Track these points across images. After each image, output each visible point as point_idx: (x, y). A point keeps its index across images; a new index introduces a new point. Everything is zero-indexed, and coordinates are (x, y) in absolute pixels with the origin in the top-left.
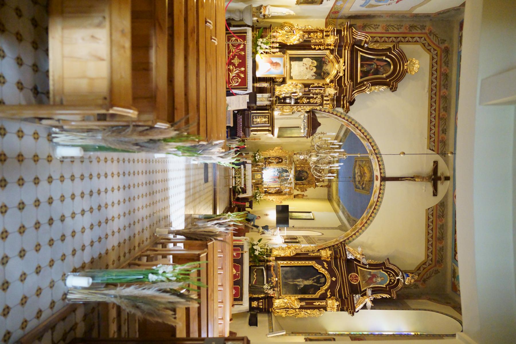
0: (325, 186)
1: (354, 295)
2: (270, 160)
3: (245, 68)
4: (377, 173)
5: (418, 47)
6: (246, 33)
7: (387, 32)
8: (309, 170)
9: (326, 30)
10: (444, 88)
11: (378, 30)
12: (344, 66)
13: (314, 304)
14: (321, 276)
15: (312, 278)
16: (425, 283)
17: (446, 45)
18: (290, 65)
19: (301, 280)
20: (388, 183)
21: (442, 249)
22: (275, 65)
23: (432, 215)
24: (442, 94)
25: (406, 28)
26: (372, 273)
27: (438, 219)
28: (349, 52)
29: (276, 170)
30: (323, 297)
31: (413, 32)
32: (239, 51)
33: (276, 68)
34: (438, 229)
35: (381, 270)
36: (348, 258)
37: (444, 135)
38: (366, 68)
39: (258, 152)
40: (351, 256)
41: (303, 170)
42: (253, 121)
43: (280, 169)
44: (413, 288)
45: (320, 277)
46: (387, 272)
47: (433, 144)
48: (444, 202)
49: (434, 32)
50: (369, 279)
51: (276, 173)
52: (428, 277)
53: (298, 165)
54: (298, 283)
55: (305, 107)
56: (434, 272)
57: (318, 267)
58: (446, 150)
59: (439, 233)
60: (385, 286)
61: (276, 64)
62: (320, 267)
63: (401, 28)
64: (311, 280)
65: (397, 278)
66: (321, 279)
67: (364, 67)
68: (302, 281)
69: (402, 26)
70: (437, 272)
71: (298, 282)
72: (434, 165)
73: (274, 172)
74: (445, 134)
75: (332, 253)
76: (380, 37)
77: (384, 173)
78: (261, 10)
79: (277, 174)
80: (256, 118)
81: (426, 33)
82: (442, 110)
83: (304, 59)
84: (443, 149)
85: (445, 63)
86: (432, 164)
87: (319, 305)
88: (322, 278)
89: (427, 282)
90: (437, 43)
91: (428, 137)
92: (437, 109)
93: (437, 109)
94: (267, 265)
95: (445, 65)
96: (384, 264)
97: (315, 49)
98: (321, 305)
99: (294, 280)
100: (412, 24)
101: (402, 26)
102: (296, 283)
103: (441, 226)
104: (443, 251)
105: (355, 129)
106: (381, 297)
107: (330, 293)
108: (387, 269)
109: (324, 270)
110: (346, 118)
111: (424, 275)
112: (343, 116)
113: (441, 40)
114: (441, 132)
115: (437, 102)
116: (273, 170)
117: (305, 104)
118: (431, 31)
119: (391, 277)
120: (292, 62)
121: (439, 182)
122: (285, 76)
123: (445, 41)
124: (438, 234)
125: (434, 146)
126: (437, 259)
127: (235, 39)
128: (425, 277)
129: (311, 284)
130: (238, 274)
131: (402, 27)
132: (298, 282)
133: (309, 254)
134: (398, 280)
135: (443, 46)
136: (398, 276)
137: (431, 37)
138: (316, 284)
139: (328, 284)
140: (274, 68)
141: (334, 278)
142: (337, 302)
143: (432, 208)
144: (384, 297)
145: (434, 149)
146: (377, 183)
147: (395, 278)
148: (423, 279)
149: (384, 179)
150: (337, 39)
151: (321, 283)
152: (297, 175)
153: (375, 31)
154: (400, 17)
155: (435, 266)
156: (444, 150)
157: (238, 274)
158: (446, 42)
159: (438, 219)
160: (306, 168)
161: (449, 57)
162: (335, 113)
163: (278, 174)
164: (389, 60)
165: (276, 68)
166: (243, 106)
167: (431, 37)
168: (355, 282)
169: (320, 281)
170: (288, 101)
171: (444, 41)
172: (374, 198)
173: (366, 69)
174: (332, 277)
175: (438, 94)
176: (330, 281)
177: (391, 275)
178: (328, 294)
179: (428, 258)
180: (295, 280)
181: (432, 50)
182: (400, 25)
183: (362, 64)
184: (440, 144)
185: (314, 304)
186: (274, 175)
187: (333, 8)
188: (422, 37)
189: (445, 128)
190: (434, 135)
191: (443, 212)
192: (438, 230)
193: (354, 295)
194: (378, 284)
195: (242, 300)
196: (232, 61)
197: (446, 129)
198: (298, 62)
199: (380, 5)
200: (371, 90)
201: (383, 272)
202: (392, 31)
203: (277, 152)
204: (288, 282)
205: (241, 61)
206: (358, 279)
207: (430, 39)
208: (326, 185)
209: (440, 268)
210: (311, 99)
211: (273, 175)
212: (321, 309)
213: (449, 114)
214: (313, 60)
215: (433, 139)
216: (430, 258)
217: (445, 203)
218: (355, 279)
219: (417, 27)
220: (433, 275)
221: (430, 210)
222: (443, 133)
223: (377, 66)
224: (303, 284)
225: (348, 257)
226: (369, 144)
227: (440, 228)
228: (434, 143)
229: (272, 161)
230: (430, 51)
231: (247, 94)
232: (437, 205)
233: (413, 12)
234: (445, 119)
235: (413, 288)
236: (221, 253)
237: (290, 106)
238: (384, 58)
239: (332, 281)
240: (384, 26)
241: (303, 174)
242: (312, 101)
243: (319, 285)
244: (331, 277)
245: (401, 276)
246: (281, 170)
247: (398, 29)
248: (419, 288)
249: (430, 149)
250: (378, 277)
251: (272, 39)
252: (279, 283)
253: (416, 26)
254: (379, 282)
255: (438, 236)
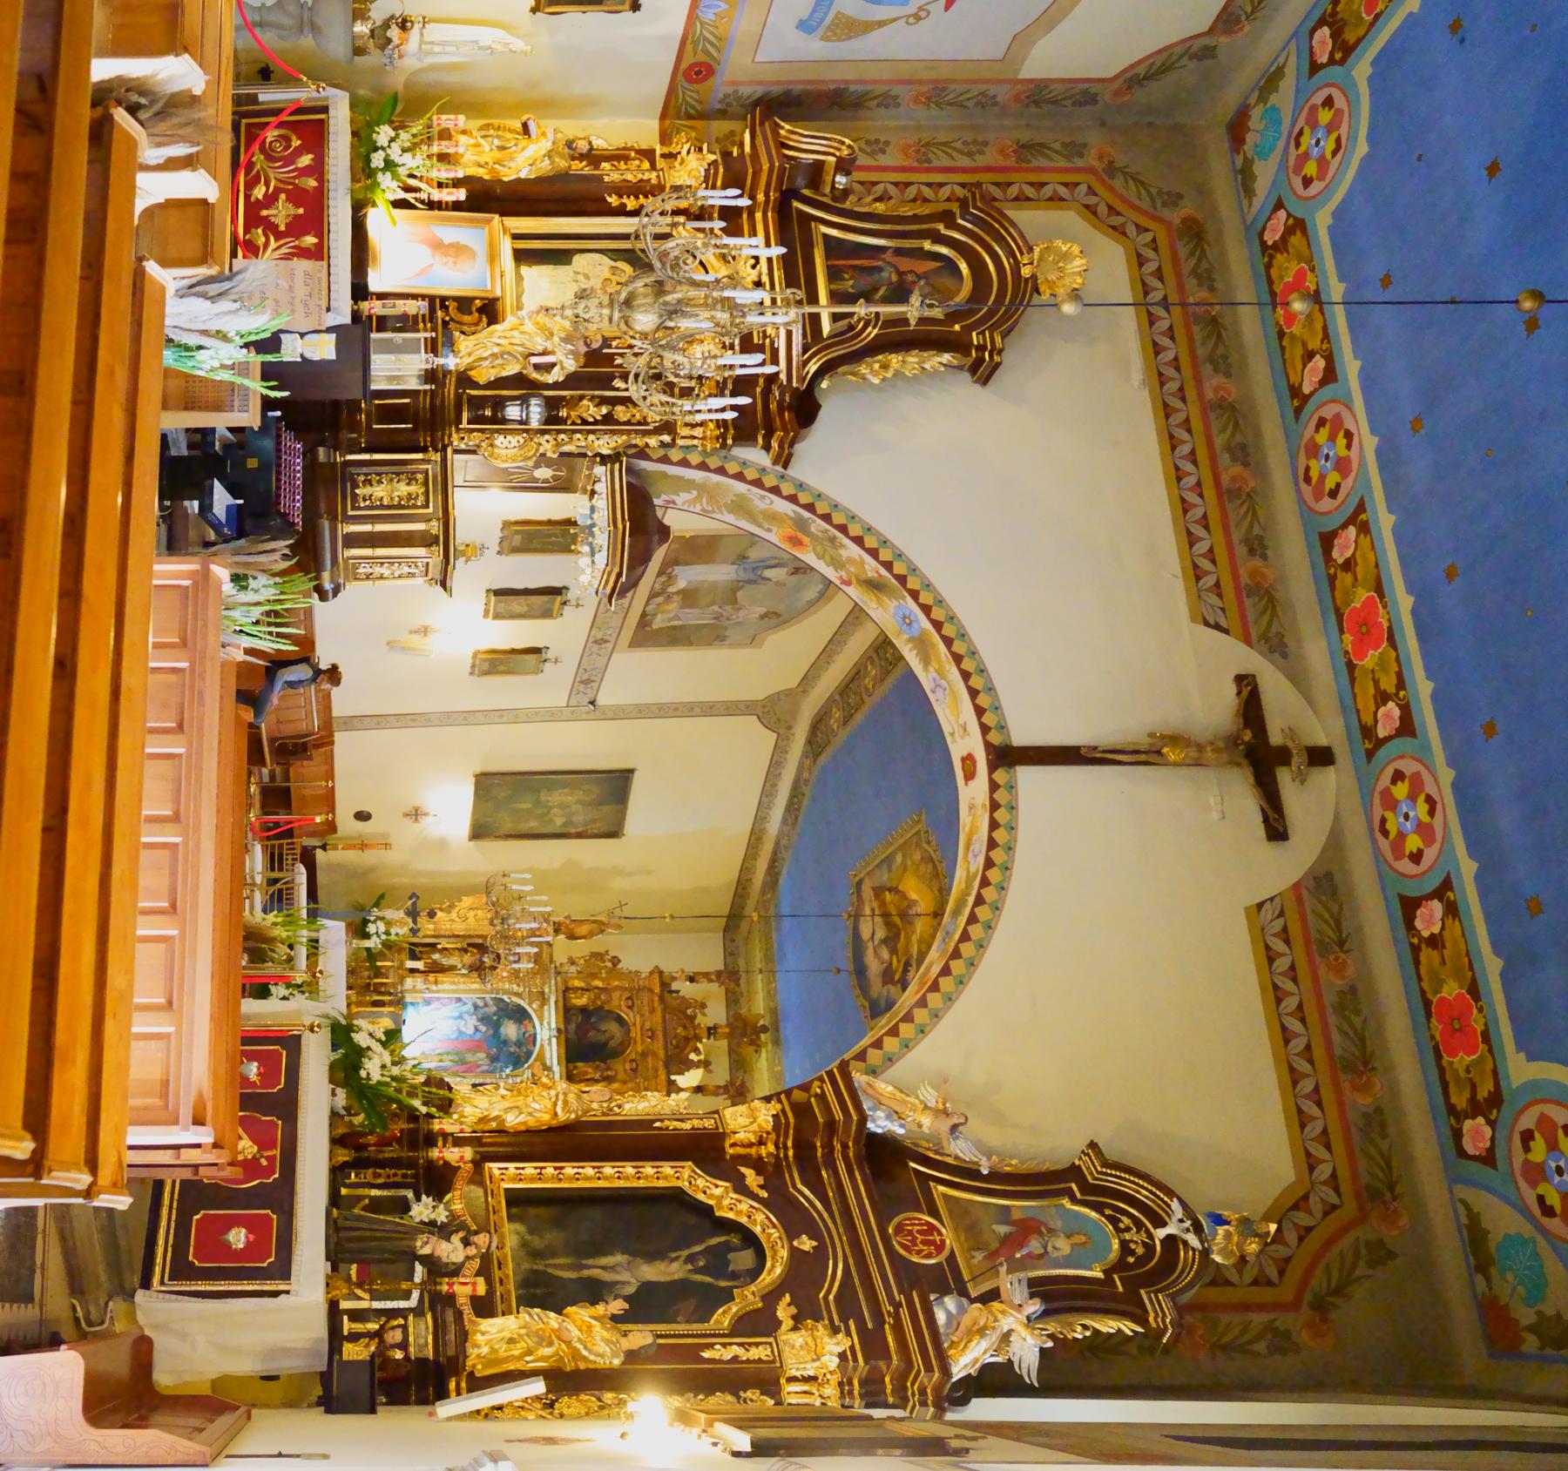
0: (718, 1087)
1: (932, 1297)
2: (436, 956)
3: (320, 235)
4: (965, 741)
5: (1070, 218)
6: (325, 110)
7: (926, 165)
8: (630, 1008)
9: (666, 150)
10: (1216, 370)
11: (883, 160)
12: (754, 267)
13: (706, 1354)
14: (735, 1240)
15: (685, 1253)
16: (1324, 1320)
17: (1187, 209)
18: (519, 278)
19: (619, 1258)
20: (1026, 775)
21: (1378, 1122)
22: (451, 252)
23: (1285, 935)
24: (1210, 395)
25: (1002, 152)
26: (1016, 1215)
27: (1318, 959)
28: (770, 214)
29: (469, 1007)
30: (759, 1324)
31: (1035, 163)
32: (294, 178)
33: (455, 263)
34: (1329, 1011)
35: (1066, 1202)
36: (871, 1126)
37: (1257, 562)
38: (851, 282)
39: (377, 905)
40: (888, 1117)
41: (601, 1007)
42: (355, 497)
43: (486, 1005)
44: (1261, 1347)
45: (727, 1248)
46: (1098, 1207)
47: (1214, 599)
48: (1329, 876)
49: (1126, 167)
50: (1006, 1240)
51: (469, 1025)
52: (1334, 1282)
53: (578, 983)
54: (608, 1277)
55: (591, 437)
56: (1363, 1251)
57: (713, 1192)
58: (1282, 626)
59: (1344, 1033)
60: (1100, 1275)
61: (457, 250)
62: (718, 1192)
63: (981, 152)
64: (677, 1258)
65: (1160, 1233)
66: (731, 1256)
67: (844, 279)
68: (629, 1267)
69: (986, 144)
70: (1381, 1254)
71: (604, 1268)
72: (1239, 694)
73: (460, 1017)
74: (1264, 557)
75: (783, 1110)
76: (896, 184)
77: (1002, 728)
78: (389, 34)
79: (471, 1031)
80: (368, 482)
81: (1090, 170)
82: (1225, 459)
83: (577, 258)
84: (1270, 624)
85: (1199, 278)
86: (1232, 689)
87: (735, 1359)
88: (736, 1250)
89: (1333, 1315)
90: (1145, 204)
91: (1184, 571)
92: (1202, 454)
93: (1202, 454)
94: (430, 1164)
95: (1200, 285)
96: (1074, 1172)
97: (621, 211)
98: (748, 1361)
99: (584, 1262)
100: (1025, 136)
101: (986, 144)
102: (595, 1272)
103: (1341, 994)
104: (1384, 1136)
105: (833, 540)
106: (1088, 1334)
107: (793, 1310)
108: (1096, 1195)
109: (745, 1204)
110: (787, 489)
111: (1309, 1272)
112: (769, 481)
113: (1160, 192)
114: (1241, 551)
115: (1197, 424)
116: (452, 1010)
117: (591, 424)
118: (1111, 163)
119: (1128, 1229)
120: (524, 270)
121: (1284, 776)
122: (498, 293)
123: (1180, 196)
124: (1336, 1038)
125: (1223, 609)
126: (1365, 1179)
127: (280, 136)
128: (1318, 1281)
129: (676, 1277)
130: (267, 1158)
131: (985, 149)
132: (604, 1268)
133: (657, 1124)
134: (1170, 1240)
135: (1175, 216)
136: (1162, 1223)
137: (1118, 183)
138: (708, 1279)
139: (774, 1271)
140: (445, 264)
141: (804, 1237)
142: (840, 1336)
143: (1277, 901)
144: (1104, 1329)
145: (1223, 623)
146: (973, 794)
147: (1150, 1236)
148: (1308, 1297)
149: (1005, 756)
150: (716, 161)
151: (734, 1276)
152: (572, 1036)
153: (873, 163)
154: (970, 104)
155: (1362, 1218)
156: (1275, 628)
157: (267, 1158)
158: (1185, 202)
159: (1318, 959)
160: (616, 995)
161: (1208, 252)
162: (732, 468)
163: (477, 1029)
164: (944, 250)
165: (455, 263)
166: (307, 315)
167: (1118, 183)
168: (929, 1256)
169: (728, 1263)
170: (513, 412)
171: (1174, 199)
172: (967, 865)
173: (852, 287)
174: (798, 1236)
175: (1191, 393)
176: (784, 1253)
177: (1126, 1220)
178: (780, 1314)
179: (1311, 1169)
180: (590, 1262)
181: (1131, 230)
182: (975, 142)
183: (834, 266)
184: (1248, 602)
185: (706, 1354)
186: (460, 1032)
187: (689, 46)
188: (1077, 185)
189: (1257, 531)
190: (1213, 561)
191: (1338, 923)
192: (1332, 1019)
193: (932, 1297)
194: (1058, 1265)
195: (286, 1275)
196: (264, 213)
197: (1260, 539)
198: (551, 267)
199: (881, 24)
200: (885, 366)
201: (1076, 1208)
202: (946, 162)
203: (471, 920)
204: (550, 1270)
205: (301, 211)
206: (943, 1242)
207: (1111, 189)
208: (722, 1083)
209: (1395, 1233)
210: (619, 408)
211: (455, 1035)
212: (749, 1394)
213: (1262, 473)
214: (615, 261)
215: (1209, 581)
216: (1324, 1171)
217: (1338, 878)
218: (924, 1242)
219: (1050, 149)
220: (1358, 1273)
221: (1268, 912)
222: (1252, 552)
223: (900, 274)
224: (633, 1280)
225: (874, 1121)
226: (909, 599)
227: (1340, 1008)
228: (1220, 596)
229: (445, 962)
230: (1124, 234)
231: (329, 330)
232: (1297, 887)
233: (1017, 71)
234: (1248, 494)
235: (1261, 1347)
236: (177, 652)
237: (526, 431)
238: (927, 245)
239: (795, 1253)
240: (909, 146)
241: (603, 1027)
242: (621, 413)
243: (723, 1284)
244: (792, 1235)
245: (1181, 1221)
246: (494, 1009)
247: (970, 155)
248: (1297, 1349)
249: (1207, 624)
250: (1051, 1231)
251: (436, 143)
252: (500, 1264)
253: (1042, 145)
254: (1065, 1257)
255: (1338, 1052)
